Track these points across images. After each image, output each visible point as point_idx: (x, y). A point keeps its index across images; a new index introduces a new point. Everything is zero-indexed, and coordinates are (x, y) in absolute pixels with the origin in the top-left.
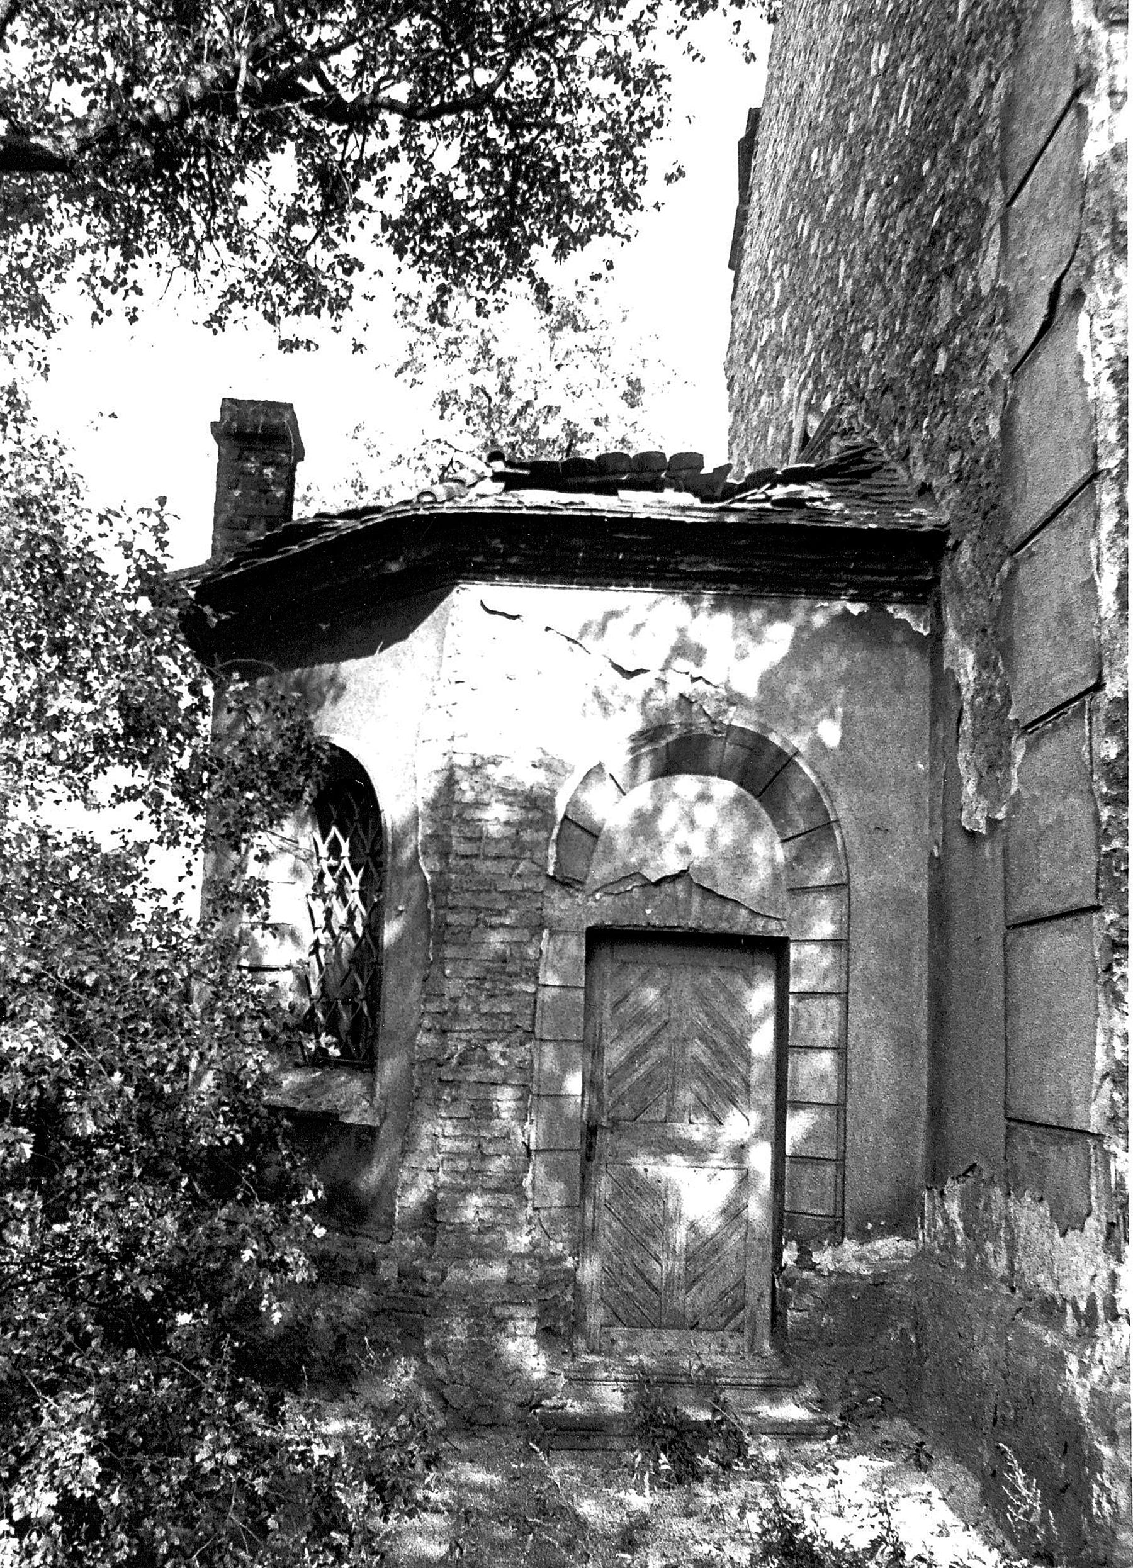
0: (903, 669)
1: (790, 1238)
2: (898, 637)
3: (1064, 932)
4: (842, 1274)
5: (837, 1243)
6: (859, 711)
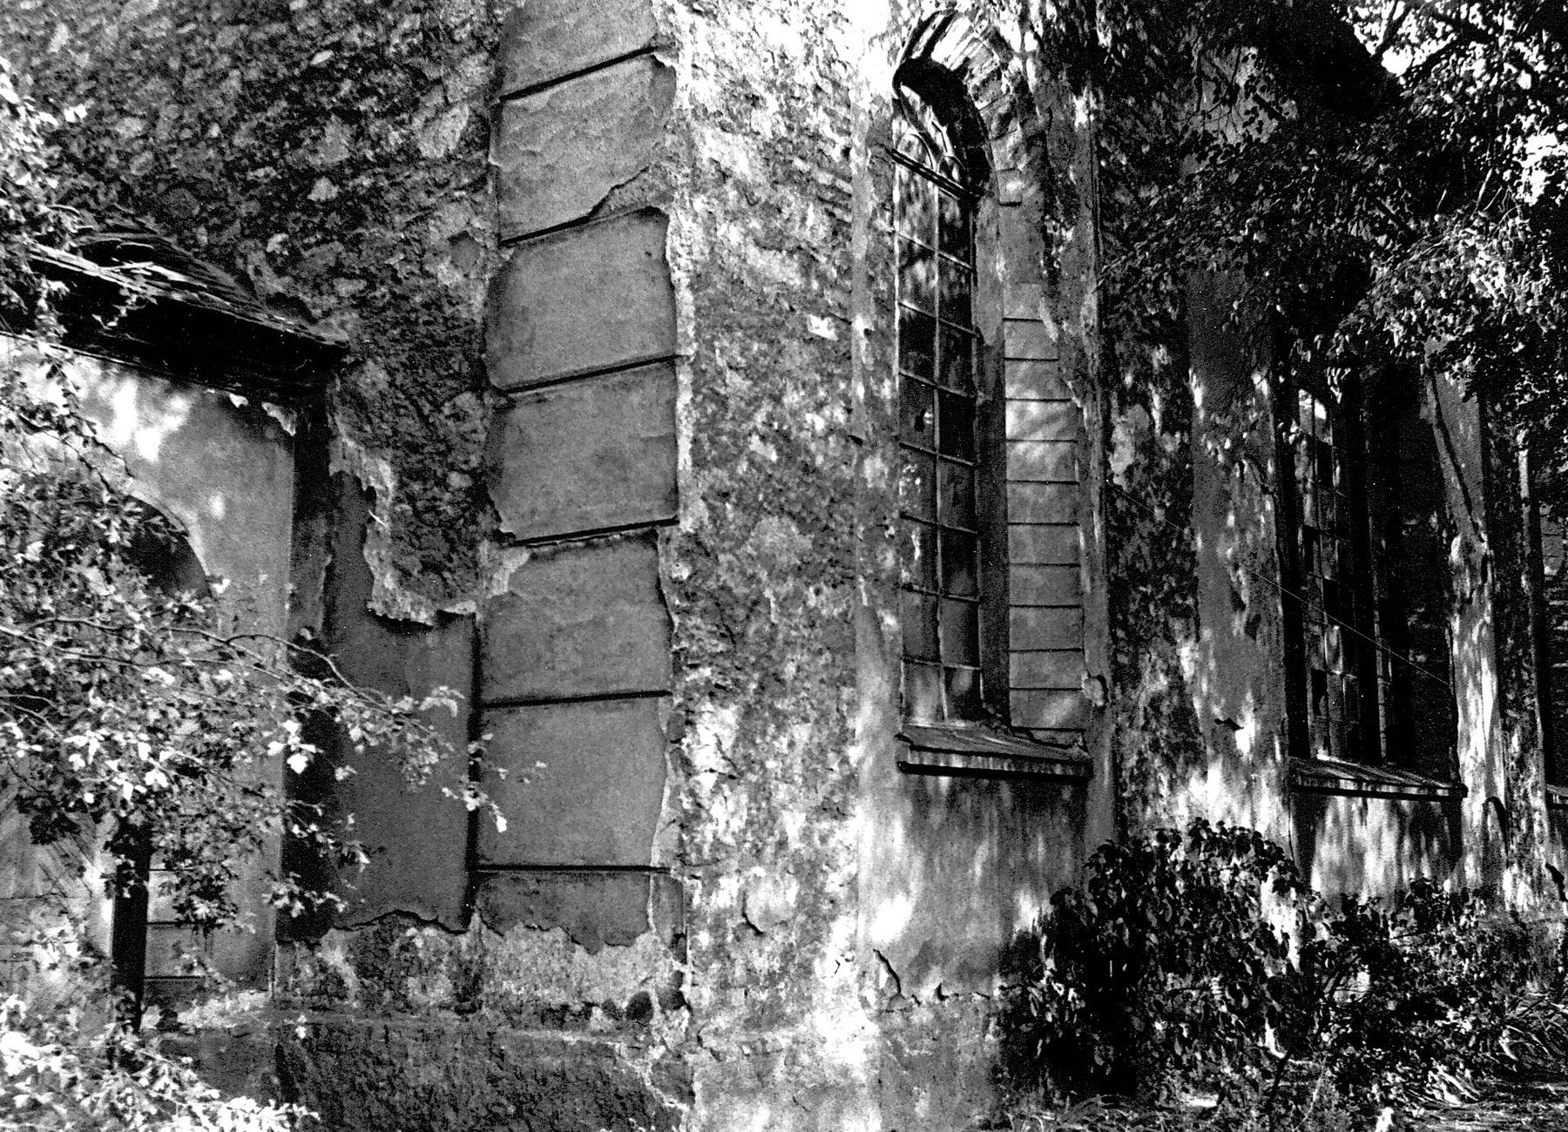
0: (272, 461)
1: (150, 1003)
2: (270, 433)
3: (598, 711)
4: (209, 1030)
5: (203, 1003)
6: (238, 499)
